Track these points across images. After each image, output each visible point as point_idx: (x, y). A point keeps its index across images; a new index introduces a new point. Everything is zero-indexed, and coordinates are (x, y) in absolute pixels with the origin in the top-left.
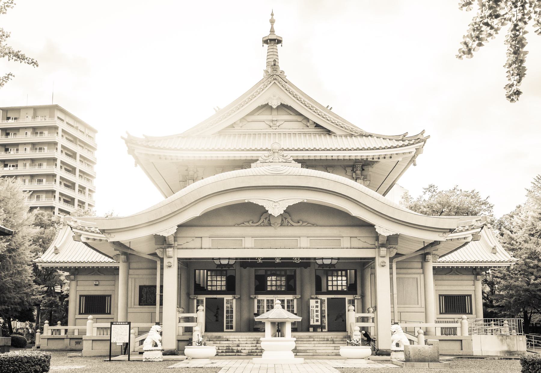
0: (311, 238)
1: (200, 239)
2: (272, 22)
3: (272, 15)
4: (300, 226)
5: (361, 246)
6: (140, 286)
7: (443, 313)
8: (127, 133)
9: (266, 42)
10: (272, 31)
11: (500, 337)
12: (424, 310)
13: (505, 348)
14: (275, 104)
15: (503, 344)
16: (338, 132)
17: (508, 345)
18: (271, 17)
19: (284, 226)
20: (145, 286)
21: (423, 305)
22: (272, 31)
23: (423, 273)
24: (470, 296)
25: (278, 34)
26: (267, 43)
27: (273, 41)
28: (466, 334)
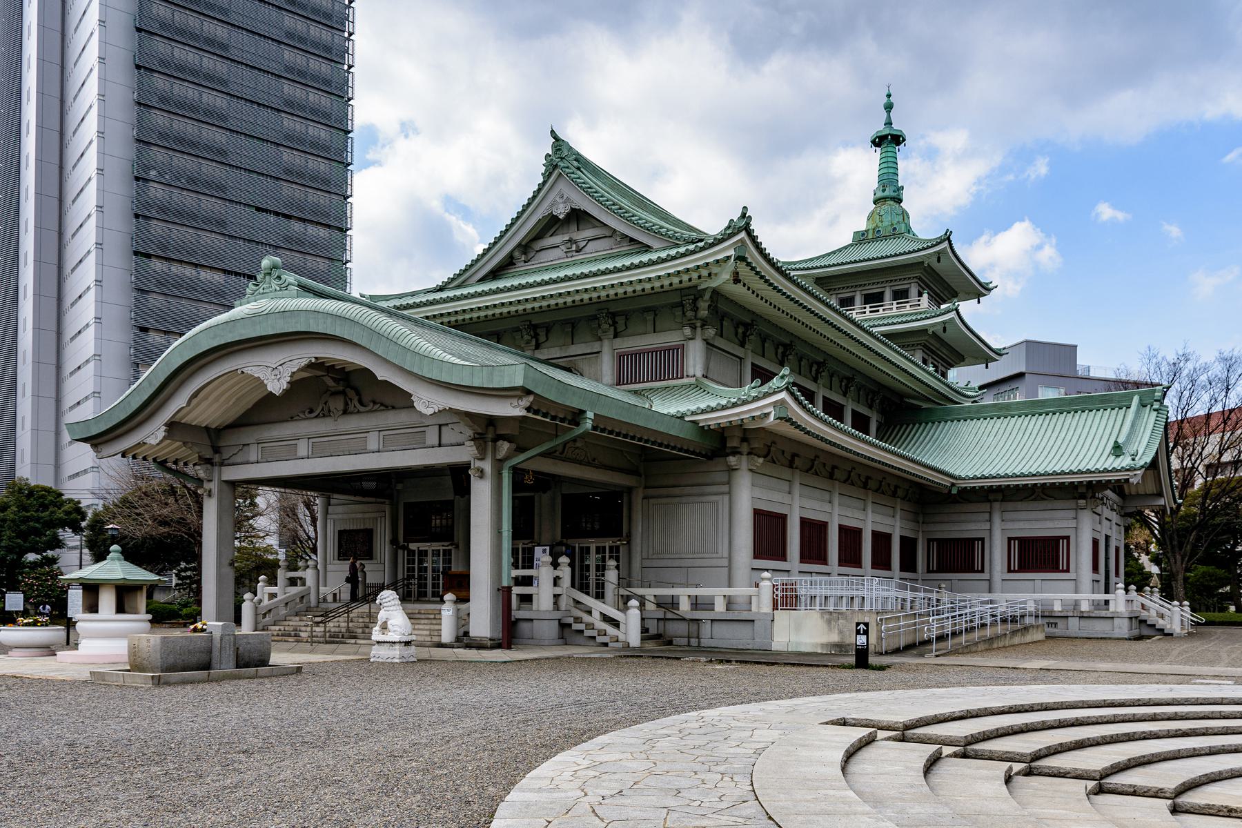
2: (889, 107)
3: (889, 96)
5: (454, 441)
10: (889, 123)
11: (827, 616)
13: (835, 638)
15: (830, 630)
17: (841, 632)
21: (726, 555)
22: (889, 123)
23: (729, 493)
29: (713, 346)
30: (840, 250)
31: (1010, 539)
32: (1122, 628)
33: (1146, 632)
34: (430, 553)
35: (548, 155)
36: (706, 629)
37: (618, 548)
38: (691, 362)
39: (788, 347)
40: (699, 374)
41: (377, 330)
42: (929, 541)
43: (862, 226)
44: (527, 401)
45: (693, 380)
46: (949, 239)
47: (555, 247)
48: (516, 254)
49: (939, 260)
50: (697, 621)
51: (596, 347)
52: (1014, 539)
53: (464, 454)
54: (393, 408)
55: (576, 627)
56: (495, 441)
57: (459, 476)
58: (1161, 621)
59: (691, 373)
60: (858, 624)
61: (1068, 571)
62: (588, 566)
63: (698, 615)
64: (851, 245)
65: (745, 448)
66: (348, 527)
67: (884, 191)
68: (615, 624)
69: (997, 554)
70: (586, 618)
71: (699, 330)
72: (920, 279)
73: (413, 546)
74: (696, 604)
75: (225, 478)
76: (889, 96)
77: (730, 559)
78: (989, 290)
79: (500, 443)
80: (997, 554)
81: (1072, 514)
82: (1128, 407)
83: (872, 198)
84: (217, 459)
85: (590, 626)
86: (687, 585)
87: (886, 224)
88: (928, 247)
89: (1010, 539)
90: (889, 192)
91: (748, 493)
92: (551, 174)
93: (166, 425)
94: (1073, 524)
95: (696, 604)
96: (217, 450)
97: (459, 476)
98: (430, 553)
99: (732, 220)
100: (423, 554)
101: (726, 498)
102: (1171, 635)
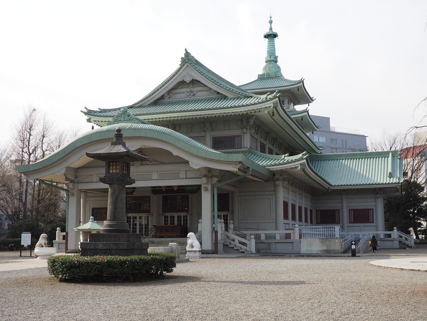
0: (161, 173)
1: (187, 177)
2: (271, 22)
3: (271, 17)
4: (153, 164)
5: (192, 176)
6: (92, 208)
7: (352, 223)
8: (86, 108)
9: (265, 37)
10: (271, 29)
11: (321, 240)
12: (274, 221)
13: (325, 248)
14: (188, 80)
15: (323, 245)
16: (230, 96)
17: (327, 246)
18: (270, 19)
19: (143, 165)
20: (96, 208)
21: (274, 218)
22: (271, 29)
23: (275, 195)
24: (372, 209)
25: (275, 30)
26: (267, 38)
27: (271, 36)
28: (297, 237)
29: (254, 137)
30: (250, 83)
31: (350, 210)
32: (396, 244)
33: (404, 246)
34: (138, 218)
35: (182, 58)
36: (273, 246)
37: (227, 216)
38: (245, 143)
39: (268, 133)
40: (249, 147)
41: (179, 138)
42: (317, 211)
43: (261, 73)
44: (238, 166)
45: (247, 149)
46: (303, 81)
47: (182, 93)
48: (166, 95)
49: (298, 90)
50: (269, 244)
51: (203, 134)
52: (351, 210)
53: (202, 181)
54: (164, 163)
55: (230, 246)
56: (211, 177)
57: (197, 189)
58: (407, 242)
59: (246, 146)
60: (352, 242)
61: (373, 222)
62: (136, 224)
63: (270, 241)
64: (257, 80)
65: (281, 178)
66: (97, 206)
67: (270, 57)
68: (244, 244)
69: (345, 216)
70: (232, 242)
71: (248, 130)
72: (289, 97)
73: (130, 215)
74: (267, 237)
75: (80, 188)
76: (271, 17)
77: (276, 219)
78: (313, 100)
79: (213, 178)
80: (345, 216)
81: (374, 200)
82: (388, 157)
83: (265, 60)
84: (76, 180)
85: (235, 245)
86: (264, 230)
87: (272, 72)
88: (294, 85)
89: (350, 210)
90: (272, 58)
91: (283, 195)
92: (184, 65)
93: (66, 168)
94: (374, 204)
95: (267, 237)
96: (76, 177)
97: (197, 189)
98: (138, 218)
99: (182, 58)
100: (135, 218)
101: (274, 197)
102: (411, 247)
